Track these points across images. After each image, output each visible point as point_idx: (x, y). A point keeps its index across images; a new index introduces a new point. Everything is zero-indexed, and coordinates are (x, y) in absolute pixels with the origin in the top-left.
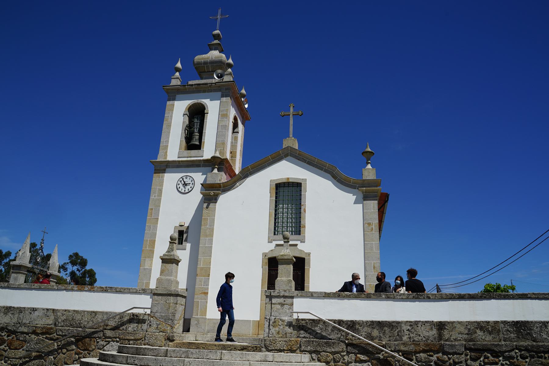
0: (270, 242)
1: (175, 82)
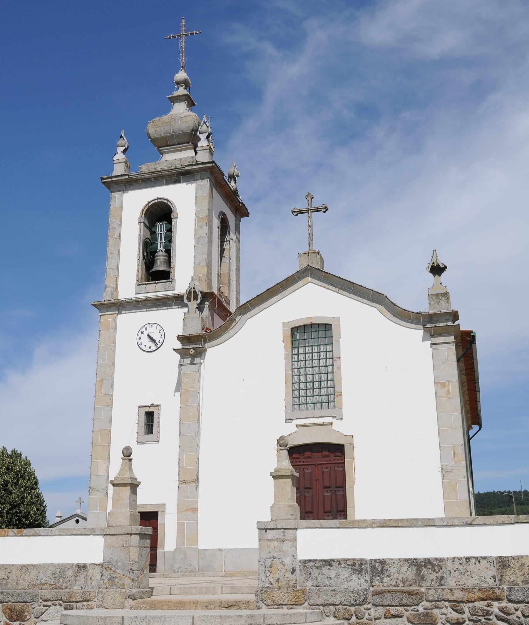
0: (289, 420)
1: (119, 170)
